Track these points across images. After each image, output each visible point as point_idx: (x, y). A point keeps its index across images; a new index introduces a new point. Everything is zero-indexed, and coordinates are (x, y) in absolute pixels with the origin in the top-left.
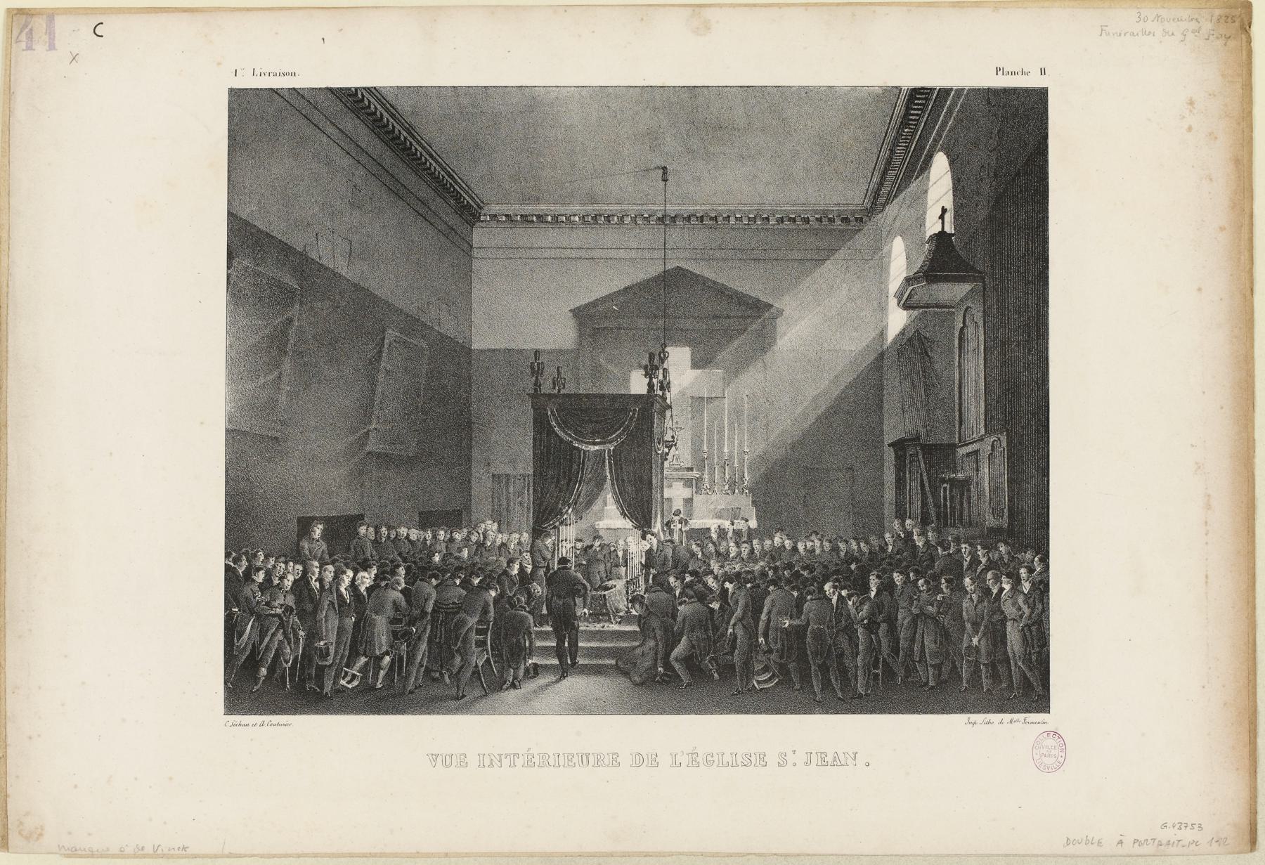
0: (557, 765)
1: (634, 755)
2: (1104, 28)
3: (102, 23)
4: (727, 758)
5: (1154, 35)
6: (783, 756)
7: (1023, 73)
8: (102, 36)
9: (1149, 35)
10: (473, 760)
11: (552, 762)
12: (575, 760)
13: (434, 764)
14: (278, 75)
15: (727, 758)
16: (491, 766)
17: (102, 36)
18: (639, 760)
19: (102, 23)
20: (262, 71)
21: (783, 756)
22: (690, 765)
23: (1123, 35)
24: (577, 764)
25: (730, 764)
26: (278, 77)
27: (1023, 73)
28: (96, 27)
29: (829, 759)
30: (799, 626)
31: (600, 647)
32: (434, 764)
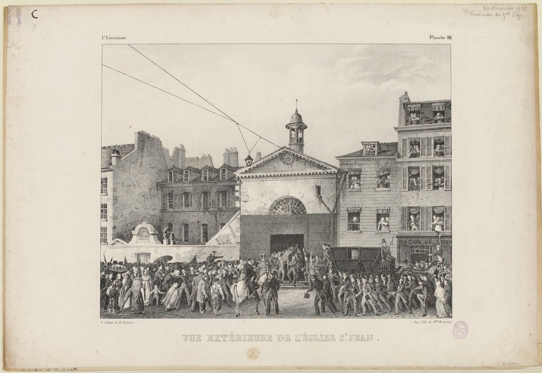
0: (224, 340)
1: (279, 336)
2: (472, 12)
3: (36, 10)
4: (319, 337)
5: (492, 15)
6: (342, 337)
7: (442, 38)
8: (37, 18)
9: (482, 14)
10: (275, 338)
11: (242, 339)
12: (220, 338)
13: (186, 339)
14: (117, 38)
15: (319, 337)
16: (368, 340)
17: (37, 18)
18: (280, 338)
19: (36, 10)
20: (110, 37)
21: (342, 337)
22: (356, 340)
23: (480, 15)
24: (254, 340)
25: (320, 340)
26: (117, 40)
27: (442, 38)
28: (33, 12)
29: (360, 338)
30: (339, 290)
31: (232, 297)
32: (186, 339)
